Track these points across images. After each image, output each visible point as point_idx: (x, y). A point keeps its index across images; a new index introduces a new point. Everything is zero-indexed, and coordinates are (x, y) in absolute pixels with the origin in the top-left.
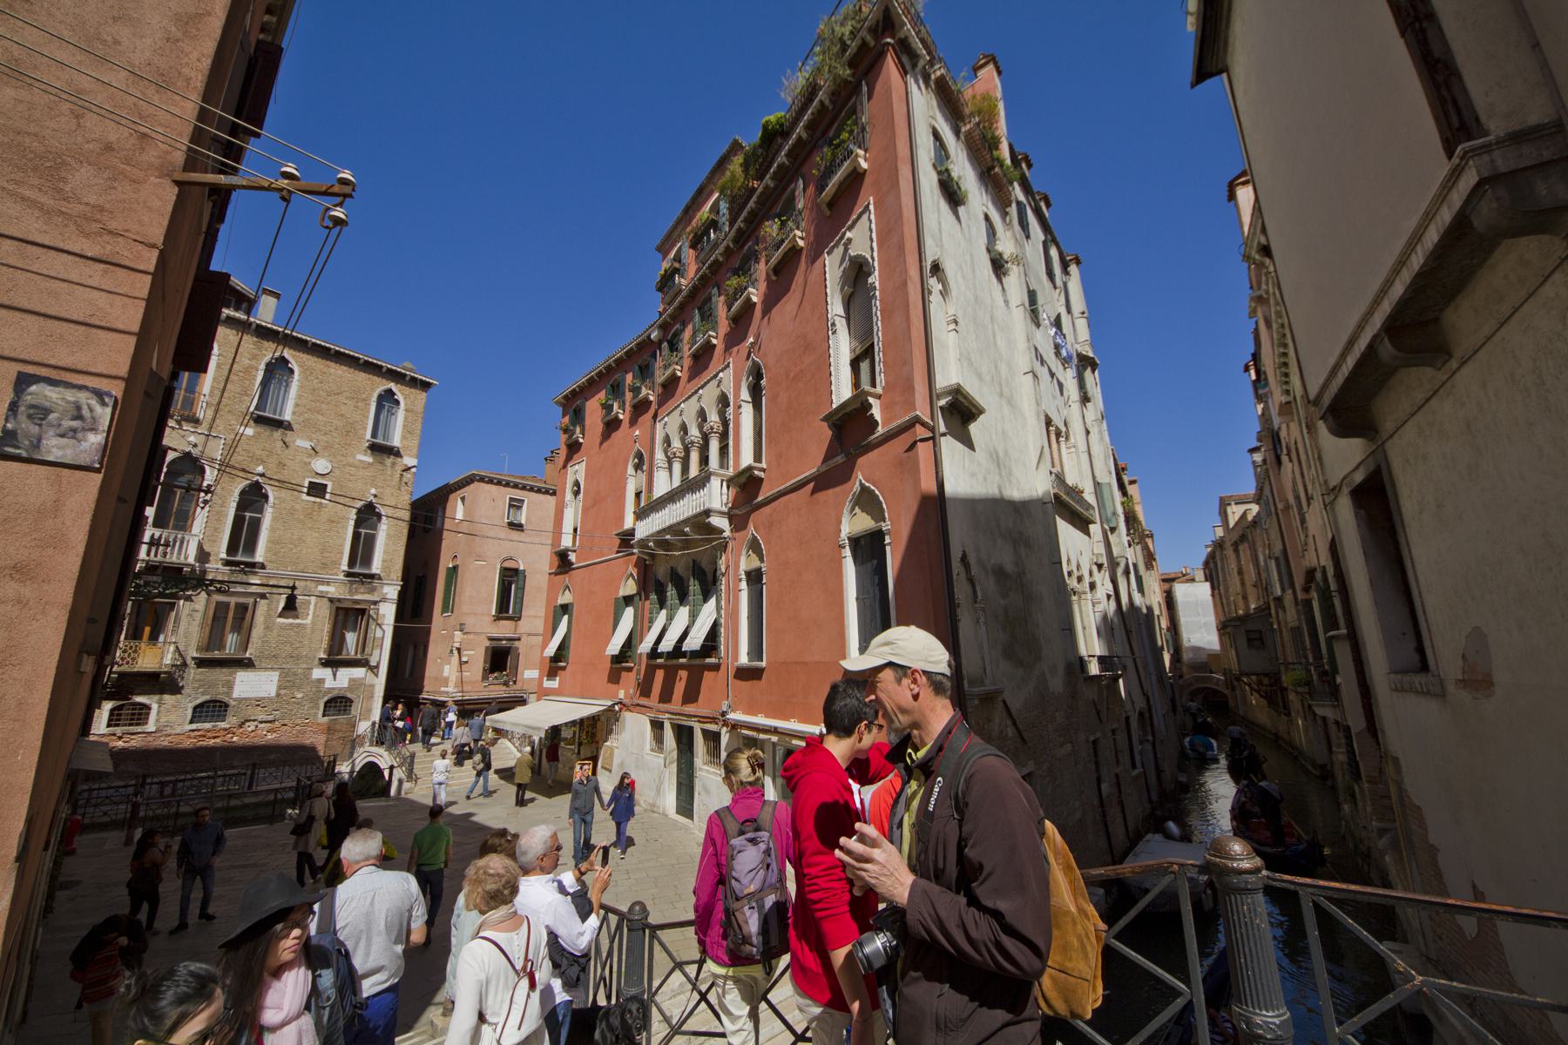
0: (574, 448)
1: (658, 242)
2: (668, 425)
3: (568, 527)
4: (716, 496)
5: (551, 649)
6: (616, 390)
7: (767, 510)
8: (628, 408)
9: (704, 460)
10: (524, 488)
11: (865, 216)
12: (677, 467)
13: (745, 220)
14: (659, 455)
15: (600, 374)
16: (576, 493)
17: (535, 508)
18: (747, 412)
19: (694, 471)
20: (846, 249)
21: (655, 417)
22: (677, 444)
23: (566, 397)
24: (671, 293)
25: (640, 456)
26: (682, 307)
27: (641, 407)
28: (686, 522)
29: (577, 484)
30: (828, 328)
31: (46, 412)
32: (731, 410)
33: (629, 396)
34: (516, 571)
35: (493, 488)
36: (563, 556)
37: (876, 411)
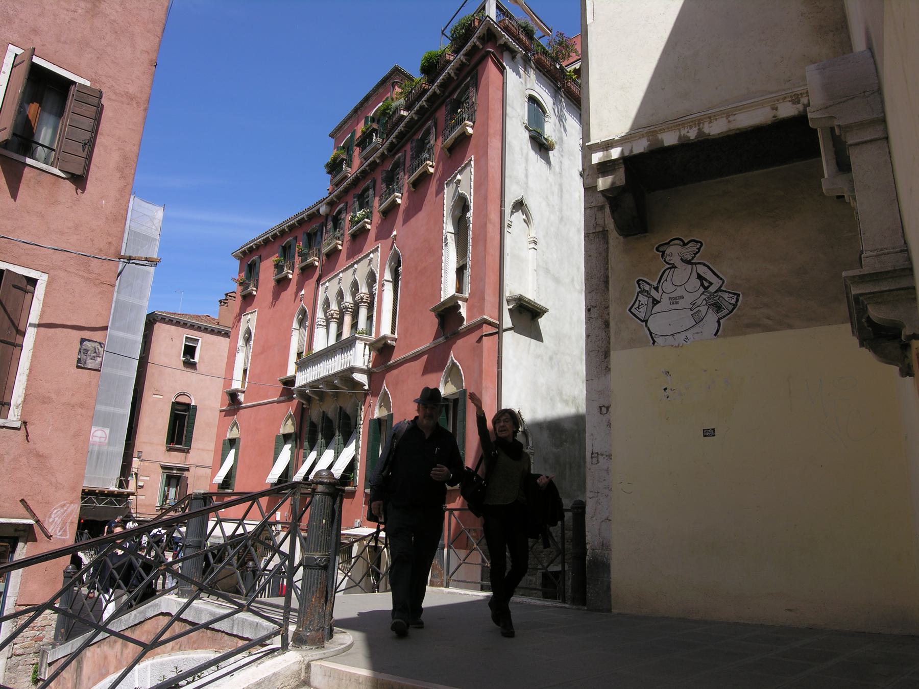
0: (248, 299)
1: (331, 129)
2: (329, 289)
3: (238, 374)
4: (359, 357)
5: (220, 477)
6: (286, 251)
7: (395, 372)
8: (297, 271)
9: (354, 325)
10: (199, 329)
11: (468, 168)
12: (333, 326)
13: (397, 137)
14: (320, 314)
15: (275, 236)
16: (247, 340)
17: (209, 348)
18: (388, 289)
19: (346, 333)
20: (457, 187)
21: (318, 281)
22: (334, 307)
23: (244, 253)
24: (339, 177)
25: (304, 312)
26: (346, 191)
27: (307, 271)
28: (335, 375)
29: (248, 332)
30: (441, 241)
31: (87, 351)
32: (376, 286)
33: (298, 259)
34: (188, 405)
35: (173, 328)
36: (233, 396)
37: (463, 311)
